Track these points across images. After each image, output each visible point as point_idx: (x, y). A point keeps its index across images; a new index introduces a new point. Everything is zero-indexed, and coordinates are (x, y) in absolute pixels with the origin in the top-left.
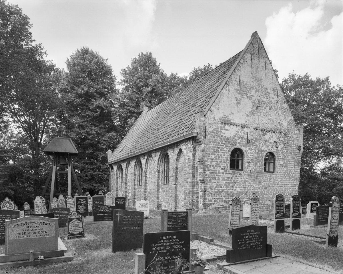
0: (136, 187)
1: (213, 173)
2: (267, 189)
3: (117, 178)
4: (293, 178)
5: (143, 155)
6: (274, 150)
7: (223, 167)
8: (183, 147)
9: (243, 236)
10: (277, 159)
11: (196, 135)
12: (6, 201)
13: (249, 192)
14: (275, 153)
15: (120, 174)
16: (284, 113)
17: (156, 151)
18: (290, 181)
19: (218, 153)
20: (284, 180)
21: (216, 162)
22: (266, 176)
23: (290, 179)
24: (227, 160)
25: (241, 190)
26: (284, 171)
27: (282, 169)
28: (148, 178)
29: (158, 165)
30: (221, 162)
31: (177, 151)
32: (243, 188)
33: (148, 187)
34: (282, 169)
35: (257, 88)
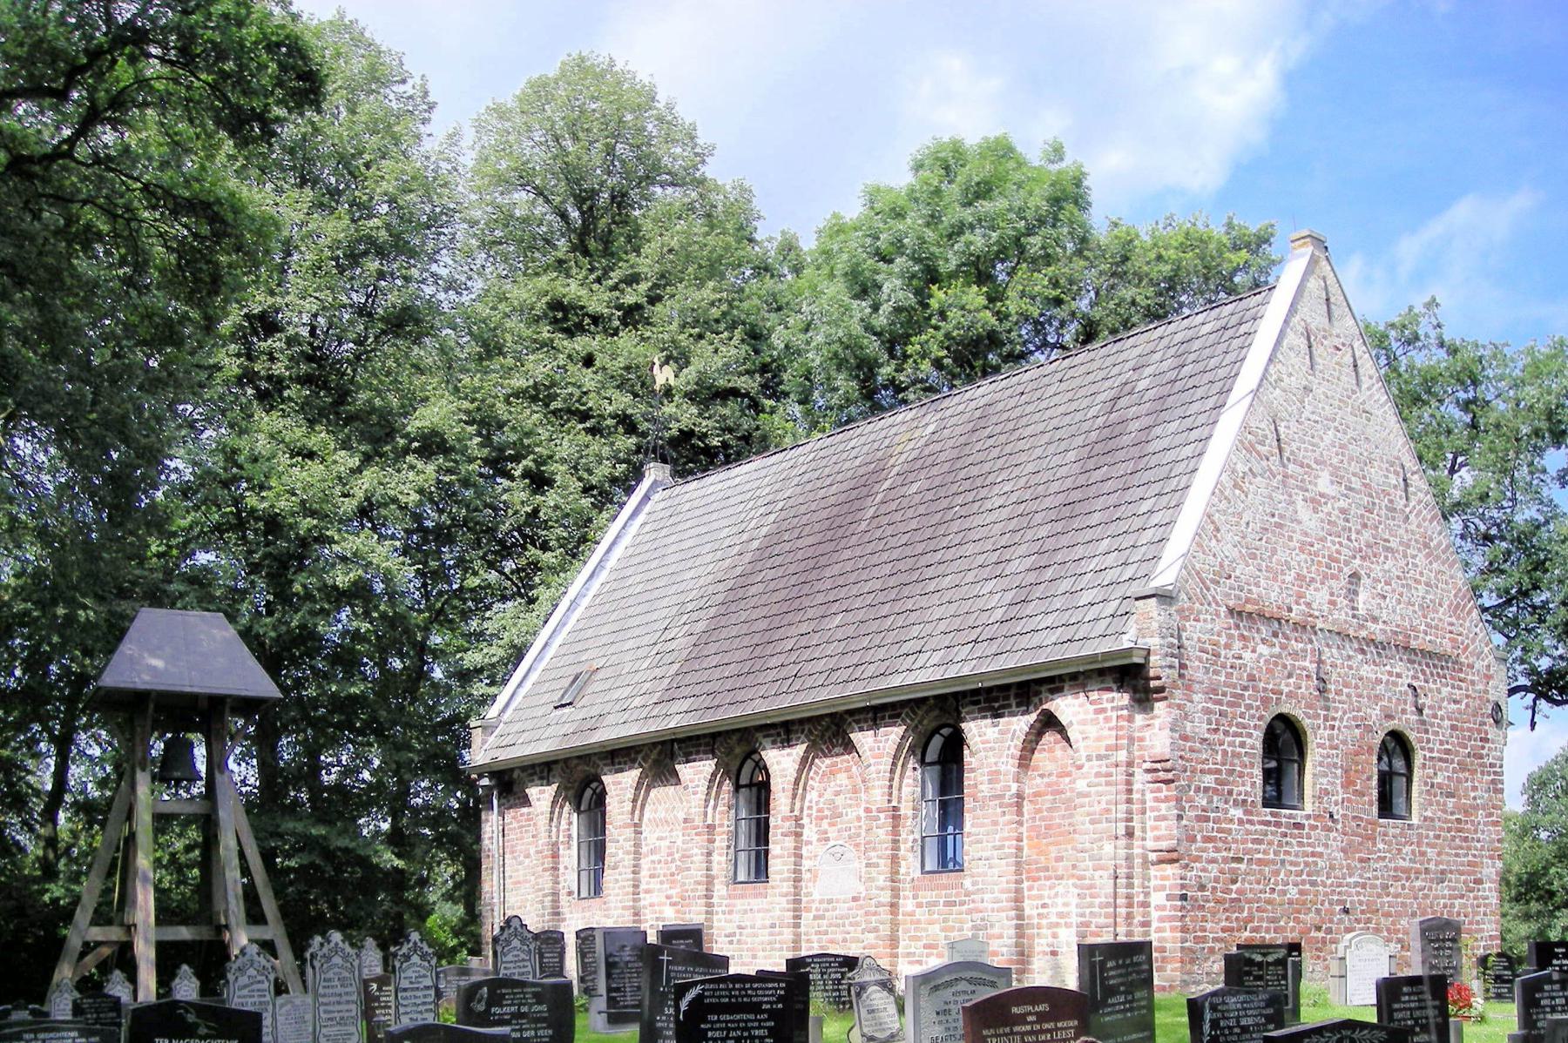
0: (720, 889)
1: (1207, 819)
2: (1392, 890)
3: (557, 843)
4: (1479, 845)
5: (784, 730)
6: (1406, 722)
7: (1240, 794)
8: (1066, 706)
9: (1540, 999)
10: (1418, 761)
11: (1141, 661)
12: (332, 945)
13: (1331, 904)
14: (1412, 736)
15: (570, 823)
16: (1435, 565)
17: (877, 714)
18: (1470, 858)
19: (1222, 736)
20: (1447, 854)
21: (1218, 772)
22: (1385, 834)
23: (1469, 848)
24: (1252, 765)
25: (1301, 893)
26: (1445, 812)
27: (1438, 803)
28: (809, 843)
29: (891, 780)
30: (1231, 772)
31: (1020, 724)
32: (1308, 886)
33: (815, 892)
34: (1438, 803)
35: (1335, 461)
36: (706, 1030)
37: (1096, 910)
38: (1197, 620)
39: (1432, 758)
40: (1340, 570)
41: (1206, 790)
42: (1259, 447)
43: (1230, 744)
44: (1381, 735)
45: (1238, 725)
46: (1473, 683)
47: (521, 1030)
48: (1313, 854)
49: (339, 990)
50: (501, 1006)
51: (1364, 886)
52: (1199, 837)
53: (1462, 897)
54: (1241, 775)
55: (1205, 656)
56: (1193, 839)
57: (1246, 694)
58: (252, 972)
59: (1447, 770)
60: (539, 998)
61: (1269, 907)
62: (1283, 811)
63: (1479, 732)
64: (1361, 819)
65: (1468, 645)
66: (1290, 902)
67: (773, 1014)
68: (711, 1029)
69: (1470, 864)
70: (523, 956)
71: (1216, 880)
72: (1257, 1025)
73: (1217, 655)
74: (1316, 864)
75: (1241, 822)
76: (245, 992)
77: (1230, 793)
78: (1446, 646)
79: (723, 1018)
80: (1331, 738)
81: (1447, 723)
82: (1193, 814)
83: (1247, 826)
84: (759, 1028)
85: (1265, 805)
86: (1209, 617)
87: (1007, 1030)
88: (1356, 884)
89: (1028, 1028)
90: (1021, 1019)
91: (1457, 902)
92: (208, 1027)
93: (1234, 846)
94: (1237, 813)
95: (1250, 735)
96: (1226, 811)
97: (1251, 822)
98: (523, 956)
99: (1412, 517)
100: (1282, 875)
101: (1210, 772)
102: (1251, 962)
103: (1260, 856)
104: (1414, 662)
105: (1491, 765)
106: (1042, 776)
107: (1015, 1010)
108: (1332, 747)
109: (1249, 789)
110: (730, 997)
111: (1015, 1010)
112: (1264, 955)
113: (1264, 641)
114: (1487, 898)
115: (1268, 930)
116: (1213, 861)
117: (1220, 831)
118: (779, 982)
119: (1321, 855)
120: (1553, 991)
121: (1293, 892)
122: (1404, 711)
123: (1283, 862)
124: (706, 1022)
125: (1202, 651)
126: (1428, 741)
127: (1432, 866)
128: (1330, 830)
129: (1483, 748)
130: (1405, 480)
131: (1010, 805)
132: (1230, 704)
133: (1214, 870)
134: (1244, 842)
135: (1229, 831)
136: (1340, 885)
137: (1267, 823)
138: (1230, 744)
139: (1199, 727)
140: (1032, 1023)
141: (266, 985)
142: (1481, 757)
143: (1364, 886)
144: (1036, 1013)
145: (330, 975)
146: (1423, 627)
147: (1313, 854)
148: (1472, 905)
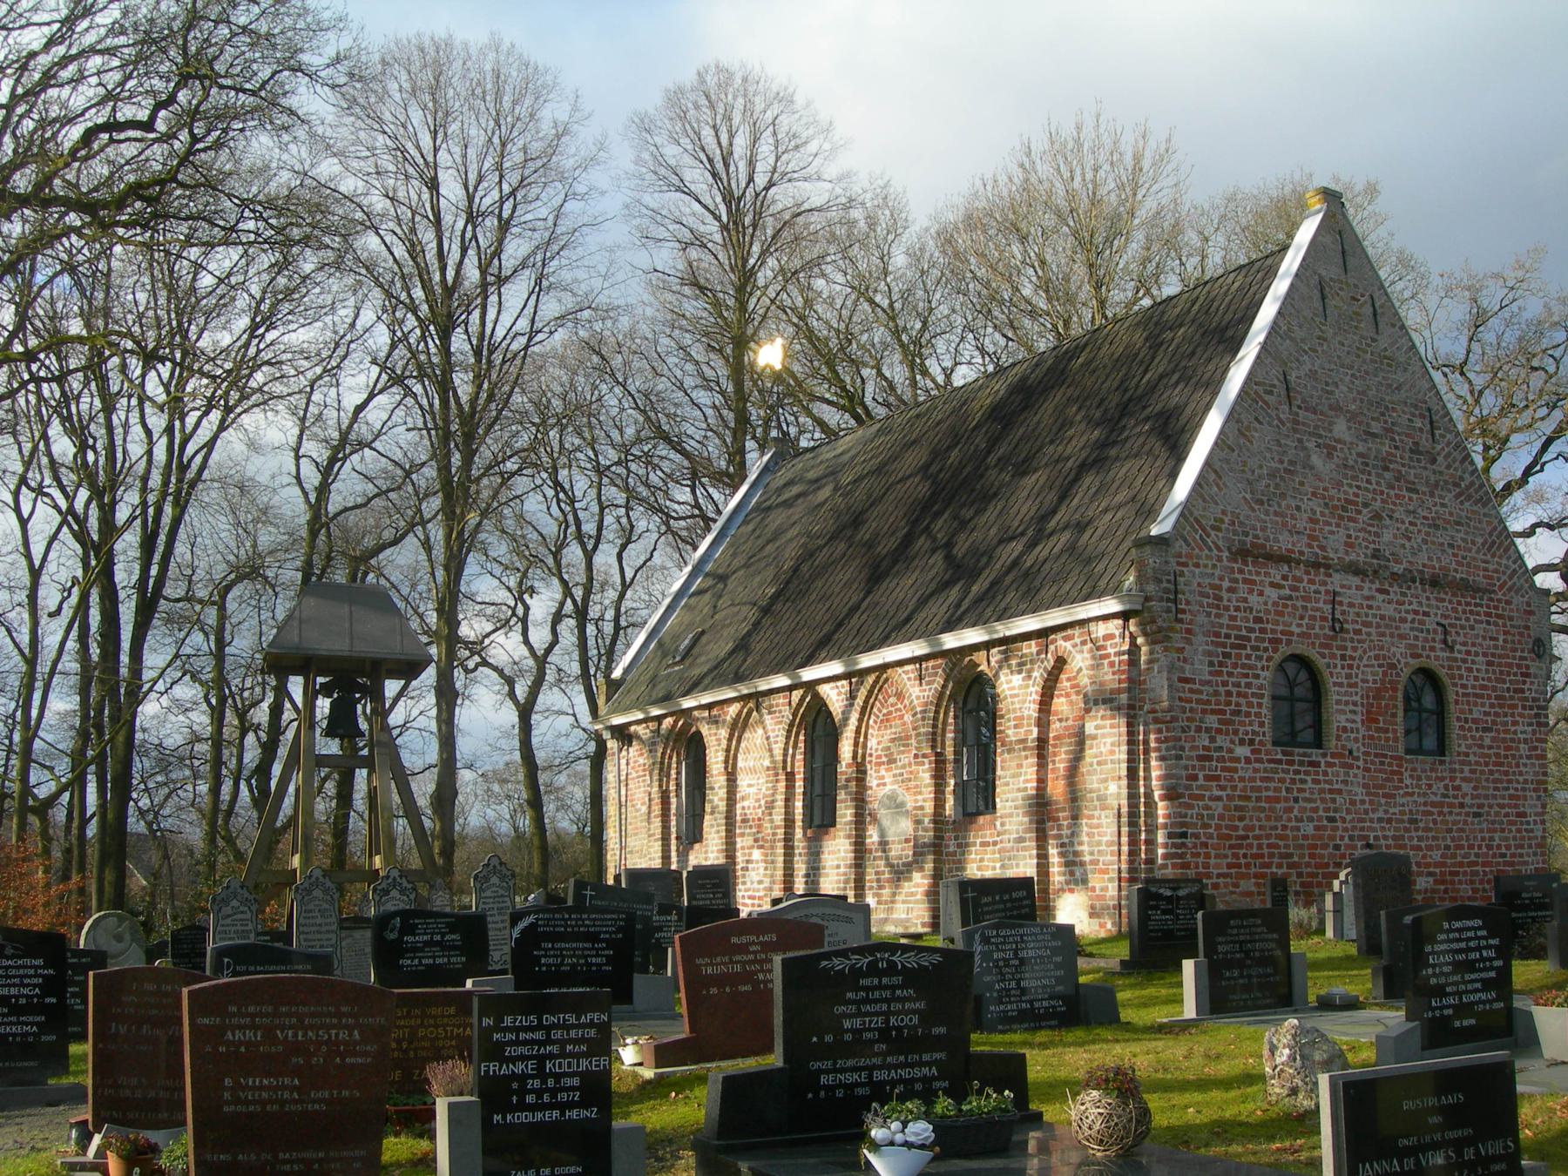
1: (1210, 759)
2: (1421, 825)
6: (1437, 660)
14: (1442, 673)
25: (1317, 828)
30: (1237, 713)
36: (539, 957)
37: (1103, 848)
38: (1197, 565)
39: (1464, 695)
40: (1359, 512)
41: (1208, 730)
42: (1266, 397)
43: (1234, 685)
44: (1407, 672)
45: (1244, 666)
46: (1511, 619)
47: (434, 957)
48: (1331, 791)
49: (318, 921)
50: (414, 935)
51: (1389, 821)
52: (1201, 776)
53: (1503, 830)
54: (1248, 714)
55: (1205, 601)
56: (1195, 778)
57: (1253, 636)
58: (235, 903)
59: (1483, 705)
60: (452, 928)
61: (1281, 843)
62: (1297, 750)
63: (1519, 666)
64: (1385, 756)
65: (1505, 583)
66: (1305, 837)
67: (611, 944)
68: (545, 956)
69: (1511, 797)
70: (501, 892)
71: (1221, 817)
72: (1041, 957)
73: (1220, 599)
74: (1334, 800)
75: (1248, 760)
76: (228, 921)
77: (1236, 732)
78: (1481, 581)
79: (557, 945)
80: (1349, 676)
81: (1480, 659)
82: (1194, 754)
83: (1257, 765)
84: (597, 956)
85: (1275, 743)
86: (1210, 563)
87: (727, 959)
88: (1380, 820)
89: (751, 957)
90: (743, 949)
91: (1497, 836)
92: (15, 948)
93: (1240, 785)
94: (1242, 751)
95: (1257, 676)
96: (1230, 751)
97: (1258, 761)
98: (501, 892)
99: (1440, 459)
100: (1296, 812)
101: (1213, 712)
102: (1159, 897)
103: (1270, 793)
104: (1443, 600)
105: (1534, 700)
106: (1060, 720)
107: (734, 940)
108: (1350, 685)
109: (1257, 729)
110: (566, 926)
111: (734, 940)
112: (1174, 889)
113: (1272, 585)
114: (1532, 831)
115: (1280, 866)
116: (1219, 798)
117: (1223, 769)
118: (619, 913)
119: (1339, 792)
120: (1255, 926)
121: (1309, 829)
122: (1432, 649)
123: (1296, 800)
124: (540, 949)
125: (1202, 594)
126: (1461, 677)
127: (1468, 800)
128: (1351, 766)
129: (1524, 683)
130: (1431, 422)
131: (1032, 749)
132: (1233, 646)
133: (1218, 808)
134: (1253, 779)
135: (1235, 770)
136: (1361, 820)
137: (1279, 762)
138: (1234, 685)
139: (1199, 668)
140: (755, 953)
141: (249, 915)
142: (1522, 691)
143: (1389, 821)
144: (760, 943)
145: (311, 906)
146: (1454, 565)
147: (1331, 791)
148: (1515, 838)
